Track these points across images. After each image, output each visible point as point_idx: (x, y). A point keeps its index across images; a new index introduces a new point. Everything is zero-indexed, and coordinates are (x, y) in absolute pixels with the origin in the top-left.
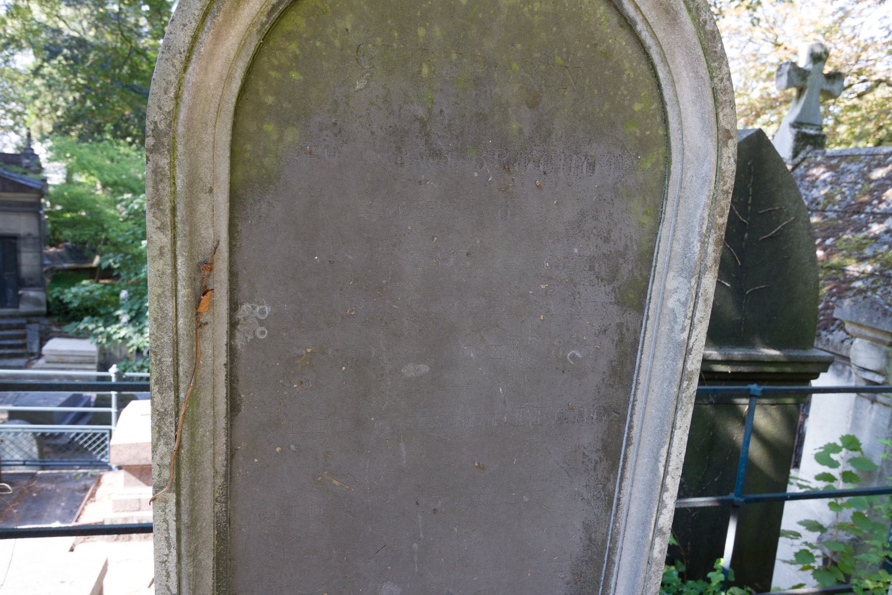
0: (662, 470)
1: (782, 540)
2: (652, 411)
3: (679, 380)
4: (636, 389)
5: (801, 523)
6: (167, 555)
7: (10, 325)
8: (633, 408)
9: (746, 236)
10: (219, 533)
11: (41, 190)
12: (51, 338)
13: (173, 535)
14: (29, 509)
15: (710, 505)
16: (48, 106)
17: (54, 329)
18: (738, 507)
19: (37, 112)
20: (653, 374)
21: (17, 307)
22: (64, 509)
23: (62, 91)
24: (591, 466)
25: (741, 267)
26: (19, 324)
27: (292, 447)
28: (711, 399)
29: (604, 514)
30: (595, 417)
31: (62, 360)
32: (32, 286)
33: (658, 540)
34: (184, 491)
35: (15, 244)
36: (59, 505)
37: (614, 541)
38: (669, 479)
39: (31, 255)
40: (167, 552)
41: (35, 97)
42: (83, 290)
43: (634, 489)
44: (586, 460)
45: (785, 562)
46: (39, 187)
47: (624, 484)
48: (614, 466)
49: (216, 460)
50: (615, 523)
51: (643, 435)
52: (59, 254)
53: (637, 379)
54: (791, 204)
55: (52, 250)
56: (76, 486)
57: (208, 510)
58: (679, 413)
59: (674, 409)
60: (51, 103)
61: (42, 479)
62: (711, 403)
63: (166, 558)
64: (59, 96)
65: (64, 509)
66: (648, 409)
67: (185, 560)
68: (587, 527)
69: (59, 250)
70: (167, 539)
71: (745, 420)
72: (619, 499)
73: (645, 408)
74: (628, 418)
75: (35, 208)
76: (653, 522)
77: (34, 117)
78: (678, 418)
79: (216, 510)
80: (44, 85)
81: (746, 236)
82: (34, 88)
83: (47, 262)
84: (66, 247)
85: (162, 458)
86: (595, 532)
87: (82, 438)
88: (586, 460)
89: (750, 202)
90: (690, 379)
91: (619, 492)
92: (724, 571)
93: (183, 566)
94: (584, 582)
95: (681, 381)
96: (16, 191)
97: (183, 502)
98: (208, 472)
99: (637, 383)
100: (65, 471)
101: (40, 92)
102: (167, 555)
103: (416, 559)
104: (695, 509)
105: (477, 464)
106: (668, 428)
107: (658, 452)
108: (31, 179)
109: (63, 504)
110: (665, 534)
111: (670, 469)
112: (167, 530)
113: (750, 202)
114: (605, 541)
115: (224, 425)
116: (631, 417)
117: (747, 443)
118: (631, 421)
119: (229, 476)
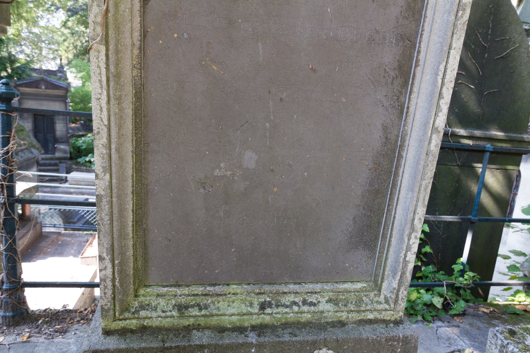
0: (440, 81)
1: (499, 259)
2: (435, 38)
3: (456, 10)
4: (424, 21)
5: (511, 251)
6: (100, 94)
7: (50, 163)
8: (421, 37)
9: (486, 55)
10: (136, 93)
11: (67, 89)
12: (72, 171)
13: (104, 79)
14: (57, 249)
15: (456, 220)
16: (71, 45)
17: (74, 167)
18: (474, 223)
19: (66, 49)
20: (437, 8)
21: (54, 154)
22: (75, 250)
23: (79, 37)
24: (390, 80)
25: (482, 76)
26: (55, 163)
27: (185, 35)
28: (458, 163)
29: (397, 120)
30: (394, 42)
31: (78, 182)
32: (62, 142)
33: (434, 136)
34: (111, 47)
35: (53, 119)
36: (73, 248)
37: (403, 140)
38: (444, 90)
39: (61, 125)
40: (100, 91)
41: (65, 40)
42: (88, 139)
43: (419, 100)
44: (386, 75)
45: (500, 273)
46: (66, 87)
47: (412, 96)
48: (405, 84)
49: (134, 35)
50: (404, 126)
51: (427, 58)
52: (77, 128)
53: (425, 14)
54: (517, 36)
55: (73, 125)
56: (83, 239)
57: (128, 73)
58: (455, 36)
59: (451, 34)
60: (73, 44)
61: (64, 235)
62: (458, 165)
63: (99, 96)
64: (77, 40)
65: (75, 250)
66: (432, 38)
67: (112, 102)
68: (385, 128)
69: (77, 125)
70: (100, 81)
71: (479, 179)
72: (408, 108)
73: (430, 36)
74: (418, 45)
75: (63, 99)
76: (432, 122)
77: (64, 52)
78: (454, 41)
79: (134, 74)
80: (70, 33)
81: (486, 55)
82: (63, 34)
83: (70, 131)
84: (81, 123)
85: (95, 17)
86: (391, 133)
87: (85, 214)
88: (386, 75)
89: (490, 32)
90: (464, 10)
91: (409, 103)
92: (463, 264)
93: (112, 105)
94: (381, 171)
95: (457, 12)
96: (53, 89)
97: (110, 56)
98: (128, 42)
99: (425, 17)
100: (76, 232)
101: (67, 38)
102: (100, 94)
103: (268, 135)
104: (446, 222)
105: (310, 67)
106: (446, 48)
107: (438, 68)
108: (62, 83)
109: (75, 248)
110: (439, 132)
111: (446, 81)
112: (100, 74)
113: (490, 32)
114: (397, 141)
115: (139, 8)
116: (420, 43)
117: (479, 193)
118: (419, 47)
119: (143, 49)
